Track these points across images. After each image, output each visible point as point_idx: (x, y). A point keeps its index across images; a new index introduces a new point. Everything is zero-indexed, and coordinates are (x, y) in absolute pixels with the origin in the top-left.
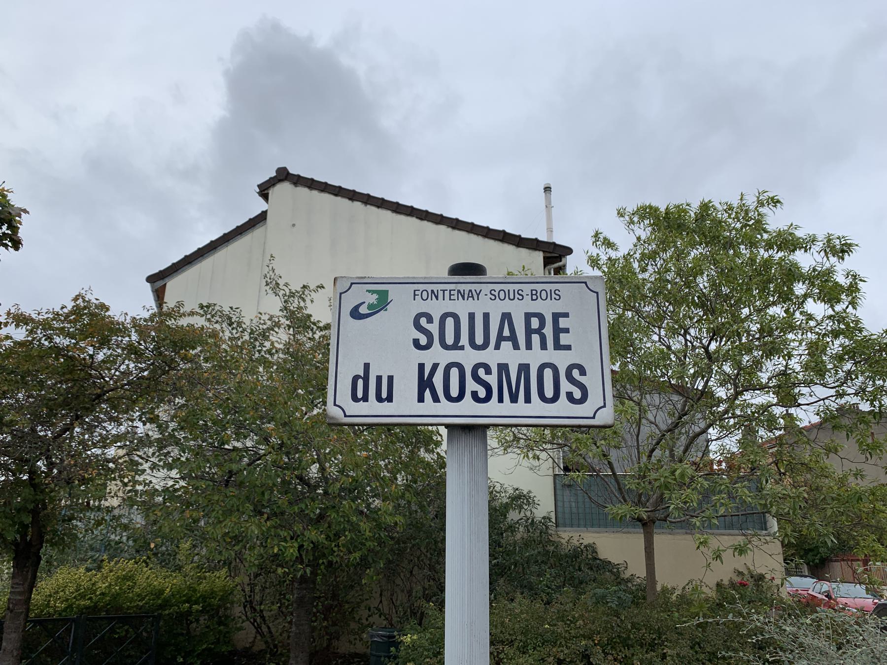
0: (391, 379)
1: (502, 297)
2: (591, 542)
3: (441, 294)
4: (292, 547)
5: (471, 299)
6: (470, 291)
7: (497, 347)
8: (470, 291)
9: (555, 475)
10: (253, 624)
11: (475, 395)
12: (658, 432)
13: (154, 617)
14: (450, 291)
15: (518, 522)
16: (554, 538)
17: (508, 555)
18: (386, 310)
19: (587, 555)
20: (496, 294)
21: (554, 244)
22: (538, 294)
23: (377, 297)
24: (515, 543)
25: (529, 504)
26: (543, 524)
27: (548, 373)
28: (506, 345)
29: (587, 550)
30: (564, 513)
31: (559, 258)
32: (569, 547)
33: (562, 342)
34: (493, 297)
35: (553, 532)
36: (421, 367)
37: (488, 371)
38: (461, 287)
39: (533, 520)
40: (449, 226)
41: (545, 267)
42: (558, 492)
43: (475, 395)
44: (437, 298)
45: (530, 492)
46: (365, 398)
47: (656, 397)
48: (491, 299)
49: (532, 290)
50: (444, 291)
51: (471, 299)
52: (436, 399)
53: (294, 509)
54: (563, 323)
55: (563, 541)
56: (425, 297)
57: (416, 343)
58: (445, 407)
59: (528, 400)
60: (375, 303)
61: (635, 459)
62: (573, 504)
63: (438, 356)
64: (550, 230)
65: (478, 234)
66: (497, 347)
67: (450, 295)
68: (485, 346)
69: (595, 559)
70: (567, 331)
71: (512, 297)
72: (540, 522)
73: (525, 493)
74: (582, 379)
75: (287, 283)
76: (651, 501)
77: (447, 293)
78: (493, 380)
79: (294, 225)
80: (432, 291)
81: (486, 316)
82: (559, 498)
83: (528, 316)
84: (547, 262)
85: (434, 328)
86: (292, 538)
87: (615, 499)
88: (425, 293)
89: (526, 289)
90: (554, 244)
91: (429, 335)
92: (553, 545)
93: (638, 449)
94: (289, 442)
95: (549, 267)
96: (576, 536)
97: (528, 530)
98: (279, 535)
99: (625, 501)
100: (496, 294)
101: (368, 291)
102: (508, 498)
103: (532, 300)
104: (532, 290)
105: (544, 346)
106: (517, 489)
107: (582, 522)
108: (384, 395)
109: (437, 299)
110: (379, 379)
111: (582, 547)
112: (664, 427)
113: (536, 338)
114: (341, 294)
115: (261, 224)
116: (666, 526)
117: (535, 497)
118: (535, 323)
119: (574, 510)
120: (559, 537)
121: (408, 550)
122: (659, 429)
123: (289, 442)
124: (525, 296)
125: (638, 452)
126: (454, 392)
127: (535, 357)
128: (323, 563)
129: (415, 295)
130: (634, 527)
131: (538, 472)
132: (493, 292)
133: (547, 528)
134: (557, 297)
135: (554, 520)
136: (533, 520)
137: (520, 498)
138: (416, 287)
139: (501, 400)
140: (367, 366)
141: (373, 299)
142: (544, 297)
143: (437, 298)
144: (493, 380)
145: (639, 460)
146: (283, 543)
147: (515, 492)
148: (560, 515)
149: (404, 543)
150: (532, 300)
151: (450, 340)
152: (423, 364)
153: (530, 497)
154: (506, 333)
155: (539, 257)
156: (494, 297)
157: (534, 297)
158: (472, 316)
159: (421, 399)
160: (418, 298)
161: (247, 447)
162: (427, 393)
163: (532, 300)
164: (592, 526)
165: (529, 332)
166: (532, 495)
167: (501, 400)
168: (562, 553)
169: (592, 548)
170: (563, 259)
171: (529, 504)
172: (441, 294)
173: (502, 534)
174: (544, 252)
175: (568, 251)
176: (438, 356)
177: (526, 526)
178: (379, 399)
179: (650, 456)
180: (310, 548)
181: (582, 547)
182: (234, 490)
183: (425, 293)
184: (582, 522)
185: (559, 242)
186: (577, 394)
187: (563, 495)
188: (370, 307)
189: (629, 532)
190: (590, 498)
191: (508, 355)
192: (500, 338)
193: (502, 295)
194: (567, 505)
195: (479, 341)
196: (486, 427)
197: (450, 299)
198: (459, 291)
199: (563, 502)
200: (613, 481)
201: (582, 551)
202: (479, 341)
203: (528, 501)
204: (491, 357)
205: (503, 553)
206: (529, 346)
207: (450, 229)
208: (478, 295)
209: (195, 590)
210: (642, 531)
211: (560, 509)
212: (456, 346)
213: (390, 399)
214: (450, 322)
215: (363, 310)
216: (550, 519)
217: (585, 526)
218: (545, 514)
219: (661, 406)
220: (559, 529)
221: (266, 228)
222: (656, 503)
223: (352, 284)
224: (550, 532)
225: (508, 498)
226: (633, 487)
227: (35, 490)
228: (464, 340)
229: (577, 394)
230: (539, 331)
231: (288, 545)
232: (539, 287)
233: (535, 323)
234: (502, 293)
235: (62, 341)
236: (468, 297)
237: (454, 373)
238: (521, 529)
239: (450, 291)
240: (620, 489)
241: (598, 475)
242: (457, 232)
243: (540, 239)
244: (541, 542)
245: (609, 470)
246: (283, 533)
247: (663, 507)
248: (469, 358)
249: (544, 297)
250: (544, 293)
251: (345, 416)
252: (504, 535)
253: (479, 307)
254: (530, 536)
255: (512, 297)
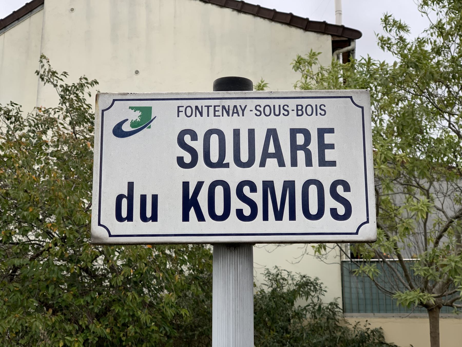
0: (155, 198)
1: (267, 112)
2: (378, 327)
3: (205, 109)
4: (77, 341)
5: (235, 115)
6: (235, 106)
7: (262, 164)
8: (235, 106)
9: (343, 262)
11: (240, 213)
12: (445, 219)
14: (215, 106)
15: (305, 308)
16: (341, 324)
17: (295, 341)
18: (150, 127)
19: (374, 340)
20: (262, 109)
21: (343, 27)
22: (304, 110)
23: (140, 114)
24: (303, 328)
25: (316, 290)
26: (330, 310)
28: (272, 162)
29: (374, 335)
30: (351, 299)
31: (348, 42)
32: (356, 332)
33: (327, 158)
34: (258, 113)
35: (340, 318)
36: (186, 185)
37: (253, 189)
38: (226, 103)
39: (320, 306)
40: (234, 9)
41: (333, 51)
42: (346, 278)
43: (240, 214)
44: (201, 114)
45: (317, 279)
46: (130, 218)
47: (444, 184)
48: (256, 114)
49: (297, 106)
50: (208, 107)
51: (235, 115)
52: (201, 218)
53: (80, 301)
54: (328, 139)
55: (350, 327)
56: (189, 113)
57: (180, 161)
59: (292, 217)
60: (138, 120)
61: (421, 246)
62: (361, 291)
64: (339, 13)
65: (264, 18)
66: (262, 164)
67: (215, 111)
68: (250, 163)
69: (382, 343)
70: (332, 146)
71: (277, 113)
72: (327, 308)
73: (312, 280)
74: (346, 195)
75: (65, 73)
76: (437, 287)
77: (211, 109)
78: (257, 197)
79: (72, 10)
80: (197, 107)
81: (251, 133)
82: (346, 284)
83: (294, 132)
84: (336, 46)
85: (198, 146)
86: (77, 332)
87: (401, 286)
88: (189, 110)
89: (292, 104)
90: (343, 28)
92: (340, 331)
93: (425, 236)
94: (72, 236)
95: (337, 52)
96: (362, 321)
97: (315, 316)
98: (65, 329)
99: (412, 287)
100: (262, 109)
101: (131, 108)
102: (296, 286)
103: (298, 115)
104: (297, 106)
105: (309, 163)
106: (304, 277)
107: (369, 307)
108: (149, 214)
109: (201, 116)
110: (143, 198)
111: (369, 332)
112: (451, 214)
113: (301, 155)
114: (103, 111)
115: (38, 9)
116: (454, 311)
117: (322, 283)
118: (300, 140)
119: (362, 296)
120: (346, 322)
121: (196, 338)
122: (446, 216)
123: (72, 236)
124: (290, 111)
125: (426, 239)
126: (219, 211)
129: (179, 111)
130: (421, 311)
131: (325, 260)
132: (258, 108)
133: (334, 314)
134: (323, 113)
135: (341, 306)
136: (320, 306)
137: (307, 285)
138: (180, 103)
139: (266, 218)
140: (131, 186)
141: (135, 116)
142: (309, 112)
143: (201, 114)
144: (257, 197)
145: (426, 246)
146: (68, 338)
147: (302, 279)
148: (347, 301)
149: (192, 330)
150: (298, 115)
151: (214, 158)
152: (188, 183)
153: (317, 284)
154: (272, 149)
155: (327, 41)
156: (259, 112)
157: (300, 113)
158: (237, 133)
159: (186, 218)
160: (182, 114)
161: (30, 241)
162: (192, 212)
163: (298, 115)
164: (379, 311)
165: (294, 148)
166: (319, 282)
167: (266, 218)
168: (349, 339)
169: (378, 333)
170: (352, 44)
171: (316, 290)
172: (205, 109)
173: (289, 320)
174: (332, 35)
175: (357, 34)
177: (314, 312)
178: (144, 218)
179: (437, 243)
180: (95, 342)
181: (369, 332)
182: (17, 285)
183: (189, 110)
184: (369, 307)
185: (347, 25)
186: (341, 210)
187: (350, 282)
188: (133, 124)
189: (415, 317)
190: (376, 285)
192: (266, 155)
193: (267, 110)
194: (354, 290)
195: (244, 158)
196: (254, 243)
197: (215, 116)
198: (224, 107)
199: (351, 288)
200: (400, 269)
201: (369, 336)
202: (244, 158)
203: (315, 288)
205: (290, 339)
206: (294, 163)
207: (235, 13)
208: (243, 111)
210: (428, 315)
211: (347, 295)
212: (221, 164)
213: (154, 218)
215: (126, 128)
216: (337, 305)
217: (372, 311)
218: (332, 300)
219: (449, 193)
220: (348, 314)
221: (44, 13)
222: (442, 289)
223: (114, 100)
224: (337, 317)
225: (296, 286)
226: (422, 273)
228: (229, 158)
229: (341, 210)
230: (304, 147)
231: (73, 339)
232: (305, 102)
233: (300, 140)
234: (267, 108)
236: (233, 113)
237: (219, 191)
238: (308, 315)
239: (215, 106)
240: (406, 276)
241: (384, 261)
242: (243, 16)
243: (329, 22)
244: (328, 328)
245: (396, 257)
246: (69, 327)
247: (450, 292)
249: (309, 112)
250: (309, 108)
251: (110, 236)
252: (292, 321)
254: (317, 323)
255: (277, 113)
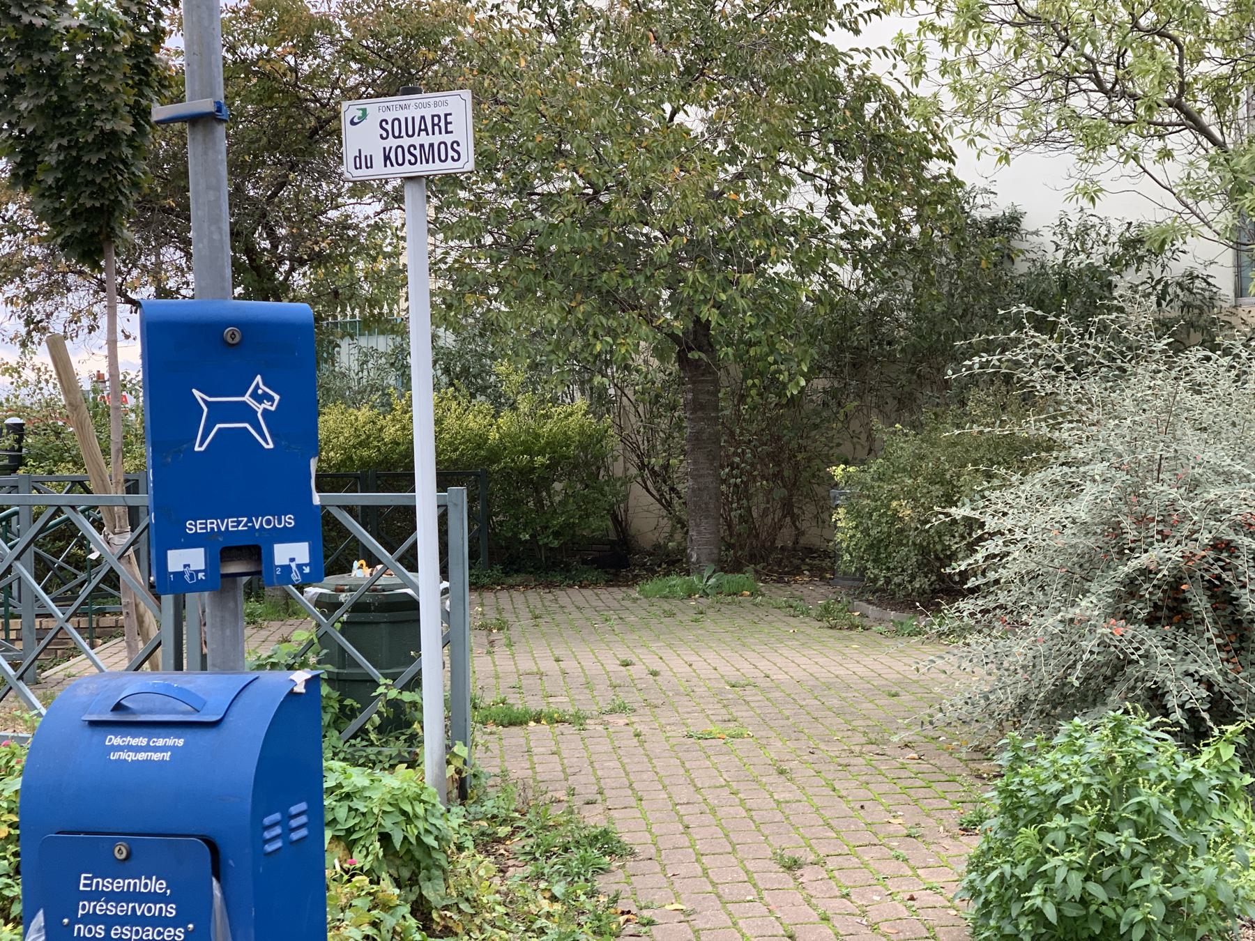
10: (659, 501)
13: (477, 475)
27: (442, 146)
28: (423, 133)
58: (397, 169)
63: (392, 142)
91: (387, 131)
113: (436, 128)
118: (436, 120)
127: (436, 139)
128: (754, 385)
144: (417, 153)
165: (433, 125)
176: (392, 142)
191: (424, 139)
192: (420, 130)
195: (410, 133)
202: (410, 133)
204: (416, 141)
209: (537, 436)
212: (400, 137)
214: (396, 123)
227: (259, 275)
228: (403, 133)
233: (436, 120)
235: (253, 52)
248: (406, 142)
253: (409, 114)
